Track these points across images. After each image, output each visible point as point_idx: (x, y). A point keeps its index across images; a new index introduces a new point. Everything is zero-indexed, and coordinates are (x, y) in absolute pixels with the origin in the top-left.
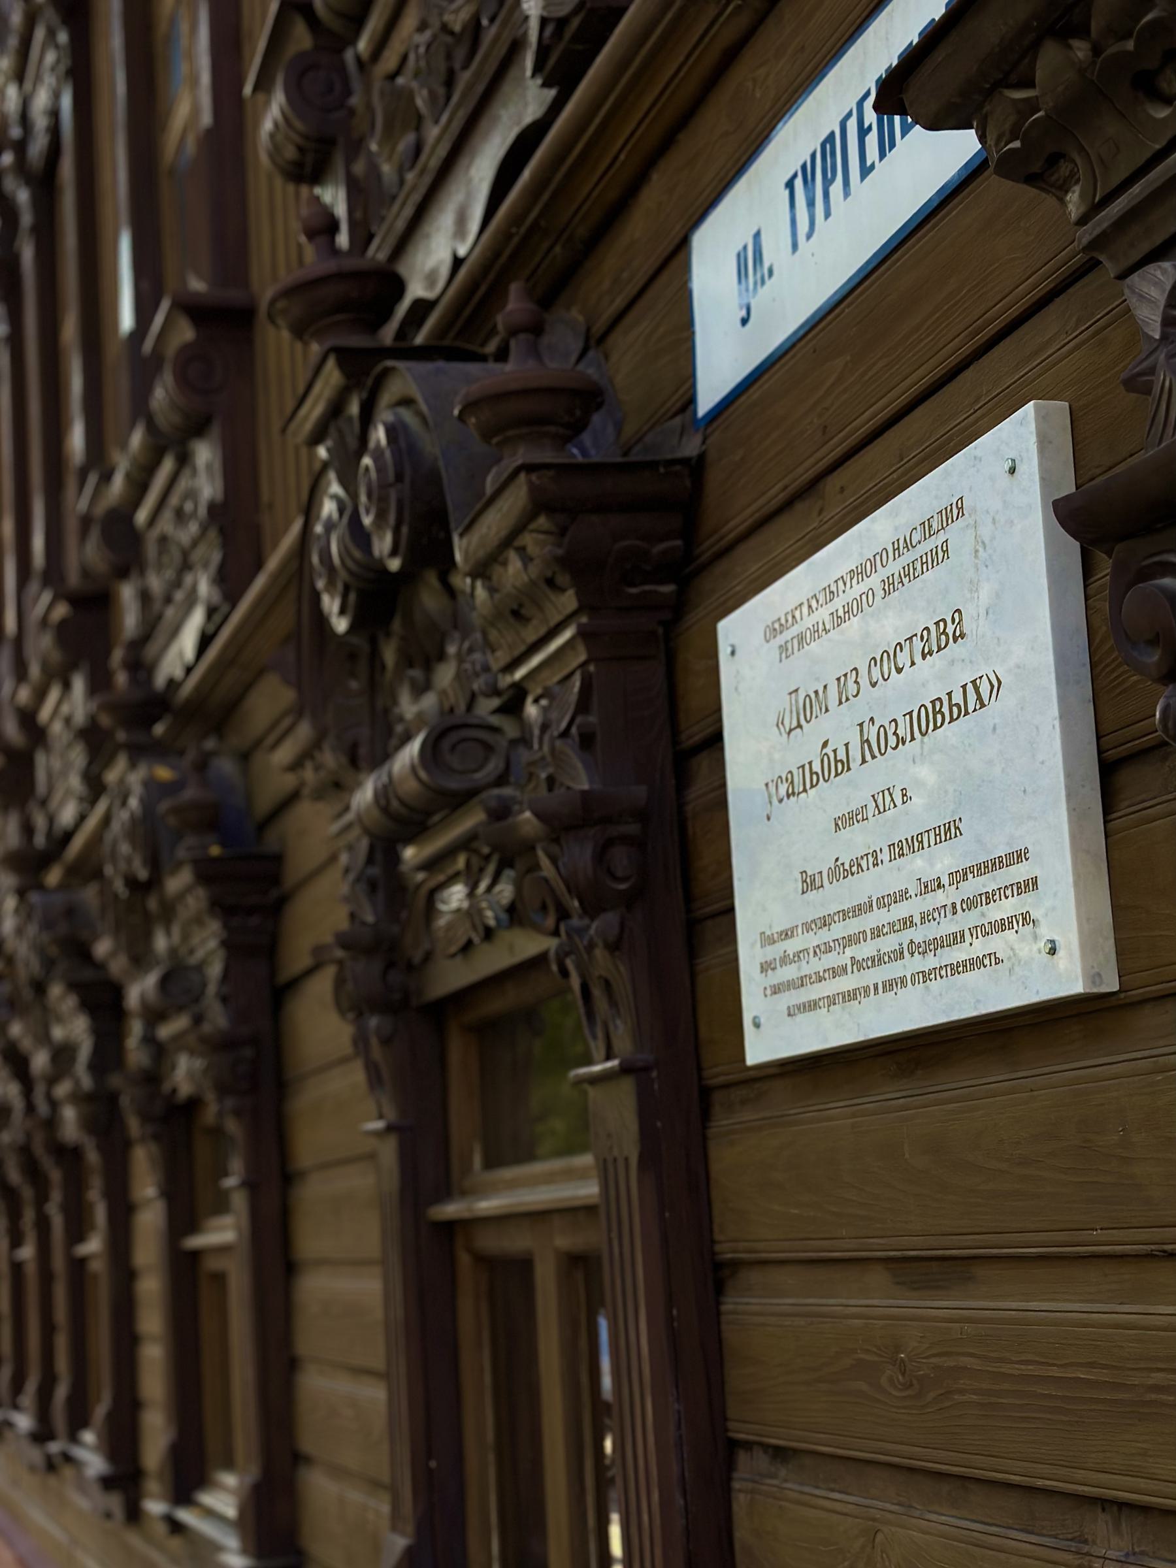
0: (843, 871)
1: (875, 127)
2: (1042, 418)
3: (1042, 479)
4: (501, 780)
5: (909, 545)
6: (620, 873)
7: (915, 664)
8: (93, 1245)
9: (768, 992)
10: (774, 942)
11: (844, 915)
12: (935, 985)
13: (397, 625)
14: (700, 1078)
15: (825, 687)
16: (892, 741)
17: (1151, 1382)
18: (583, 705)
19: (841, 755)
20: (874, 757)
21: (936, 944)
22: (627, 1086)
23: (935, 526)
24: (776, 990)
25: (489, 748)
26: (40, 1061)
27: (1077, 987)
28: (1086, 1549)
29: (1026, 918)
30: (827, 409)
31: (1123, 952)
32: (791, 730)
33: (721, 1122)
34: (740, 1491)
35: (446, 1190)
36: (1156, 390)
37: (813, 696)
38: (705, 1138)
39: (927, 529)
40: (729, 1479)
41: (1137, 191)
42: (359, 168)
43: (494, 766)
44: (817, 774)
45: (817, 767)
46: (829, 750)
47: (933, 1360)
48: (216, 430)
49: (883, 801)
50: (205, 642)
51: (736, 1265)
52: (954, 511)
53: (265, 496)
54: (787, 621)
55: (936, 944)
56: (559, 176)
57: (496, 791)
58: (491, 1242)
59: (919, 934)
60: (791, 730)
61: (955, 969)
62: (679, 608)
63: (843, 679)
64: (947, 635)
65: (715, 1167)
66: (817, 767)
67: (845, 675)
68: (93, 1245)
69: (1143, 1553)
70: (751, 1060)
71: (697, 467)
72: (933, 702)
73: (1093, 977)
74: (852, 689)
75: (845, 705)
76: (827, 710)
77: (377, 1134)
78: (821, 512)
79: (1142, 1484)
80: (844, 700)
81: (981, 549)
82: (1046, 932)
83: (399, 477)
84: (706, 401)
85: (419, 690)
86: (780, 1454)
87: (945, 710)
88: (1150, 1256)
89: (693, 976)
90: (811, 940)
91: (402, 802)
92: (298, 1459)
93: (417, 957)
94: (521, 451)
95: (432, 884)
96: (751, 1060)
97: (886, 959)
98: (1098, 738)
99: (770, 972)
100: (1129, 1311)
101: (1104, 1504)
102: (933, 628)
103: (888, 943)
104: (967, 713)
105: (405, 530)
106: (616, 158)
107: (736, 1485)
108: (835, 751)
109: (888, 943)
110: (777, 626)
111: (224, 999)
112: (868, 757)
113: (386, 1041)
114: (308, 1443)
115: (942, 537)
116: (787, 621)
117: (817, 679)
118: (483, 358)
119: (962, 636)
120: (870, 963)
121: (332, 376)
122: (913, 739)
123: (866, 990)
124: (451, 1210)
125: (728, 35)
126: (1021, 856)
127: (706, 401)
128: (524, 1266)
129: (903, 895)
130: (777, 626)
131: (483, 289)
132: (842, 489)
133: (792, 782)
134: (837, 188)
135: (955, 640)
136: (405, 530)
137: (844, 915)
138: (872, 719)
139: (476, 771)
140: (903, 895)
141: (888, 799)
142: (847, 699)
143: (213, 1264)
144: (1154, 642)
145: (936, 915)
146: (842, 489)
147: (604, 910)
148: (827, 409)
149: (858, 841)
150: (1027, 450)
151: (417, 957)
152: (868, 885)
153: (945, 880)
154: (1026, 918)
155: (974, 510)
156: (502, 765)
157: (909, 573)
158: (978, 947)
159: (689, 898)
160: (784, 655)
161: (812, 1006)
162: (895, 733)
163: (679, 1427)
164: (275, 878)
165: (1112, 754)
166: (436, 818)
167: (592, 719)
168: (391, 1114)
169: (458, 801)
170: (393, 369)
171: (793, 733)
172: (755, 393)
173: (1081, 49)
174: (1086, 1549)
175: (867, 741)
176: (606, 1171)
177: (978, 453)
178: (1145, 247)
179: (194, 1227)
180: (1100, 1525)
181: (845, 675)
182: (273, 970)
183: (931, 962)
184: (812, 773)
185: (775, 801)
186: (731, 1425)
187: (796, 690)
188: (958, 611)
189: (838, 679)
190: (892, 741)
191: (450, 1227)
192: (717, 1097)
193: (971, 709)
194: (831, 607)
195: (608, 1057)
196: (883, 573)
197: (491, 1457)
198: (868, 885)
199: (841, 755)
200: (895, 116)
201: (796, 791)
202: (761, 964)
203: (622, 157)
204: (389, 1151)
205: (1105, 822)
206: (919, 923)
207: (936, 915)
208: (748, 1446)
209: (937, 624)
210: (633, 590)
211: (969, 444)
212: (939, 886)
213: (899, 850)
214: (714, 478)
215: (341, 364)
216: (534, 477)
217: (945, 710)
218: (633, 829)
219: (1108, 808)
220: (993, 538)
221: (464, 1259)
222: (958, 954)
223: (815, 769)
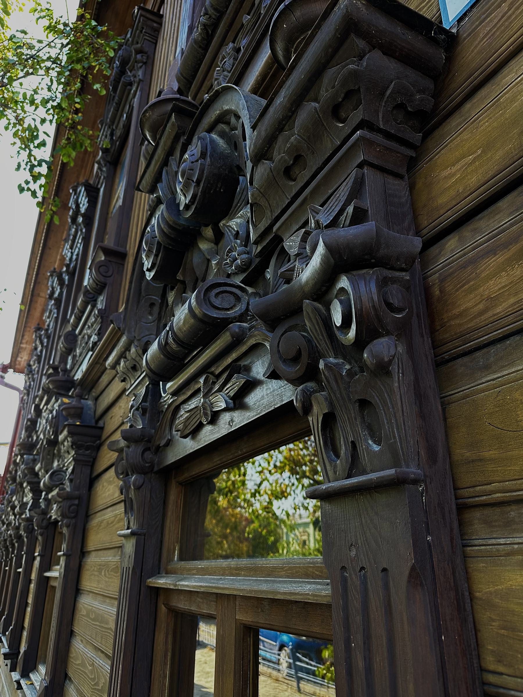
7: (150, 442)
8: (55, 573)
25: (238, 299)
26: (45, 479)
35: (157, 571)
58: (183, 605)
68: (55, 573)
77: (125, 536)
111: (71, 481)
113: (138, 488)
124: (162, 582)
143: (53, 583)
166: (54, 488)
167: (148, 404)
168: (134, 526)
179: (49, 569)
191: (157, 591)
195: (128, 529)
204: (130, 547)
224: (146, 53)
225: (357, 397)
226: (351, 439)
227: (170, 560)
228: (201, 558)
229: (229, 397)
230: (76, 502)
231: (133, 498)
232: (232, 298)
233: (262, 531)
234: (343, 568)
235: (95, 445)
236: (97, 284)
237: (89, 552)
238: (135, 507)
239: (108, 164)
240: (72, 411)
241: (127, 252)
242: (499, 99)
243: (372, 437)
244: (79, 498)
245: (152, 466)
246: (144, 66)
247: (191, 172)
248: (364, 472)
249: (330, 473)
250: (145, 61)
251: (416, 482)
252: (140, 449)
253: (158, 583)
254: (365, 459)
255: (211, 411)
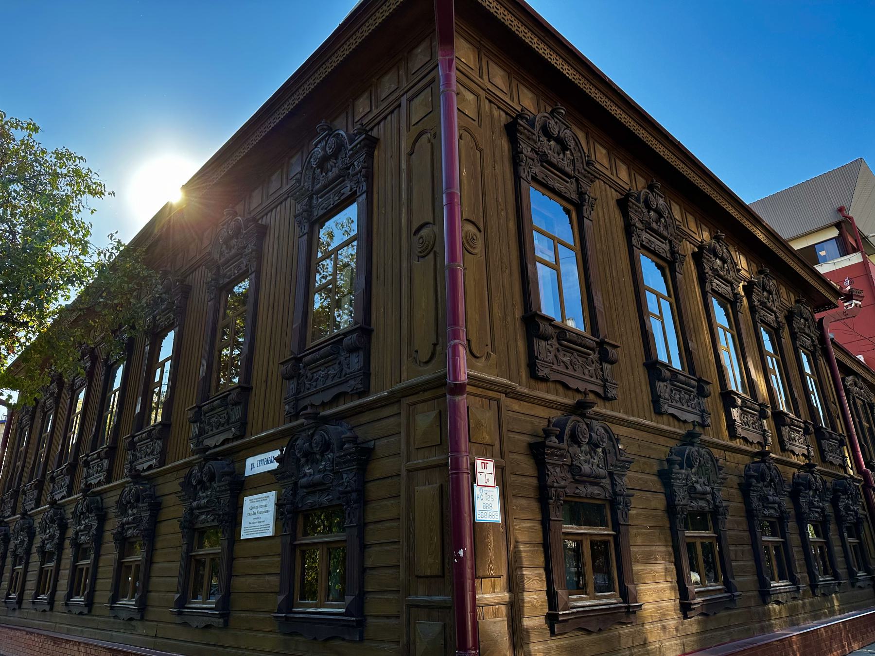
22: (227, 541)
49: (258, 518)
51: (235, 558)
52: (268, 497)
71: (244, 481)
84: (245, 475)
127: (245, 475)
128: (83, 569)
149: (256, 521)
152: (256, 524)
170: (290, 356)
176: (222, 549)
191: (192, 556)
198: (256, 524)
200: (248, 472)
211: (644, 347)
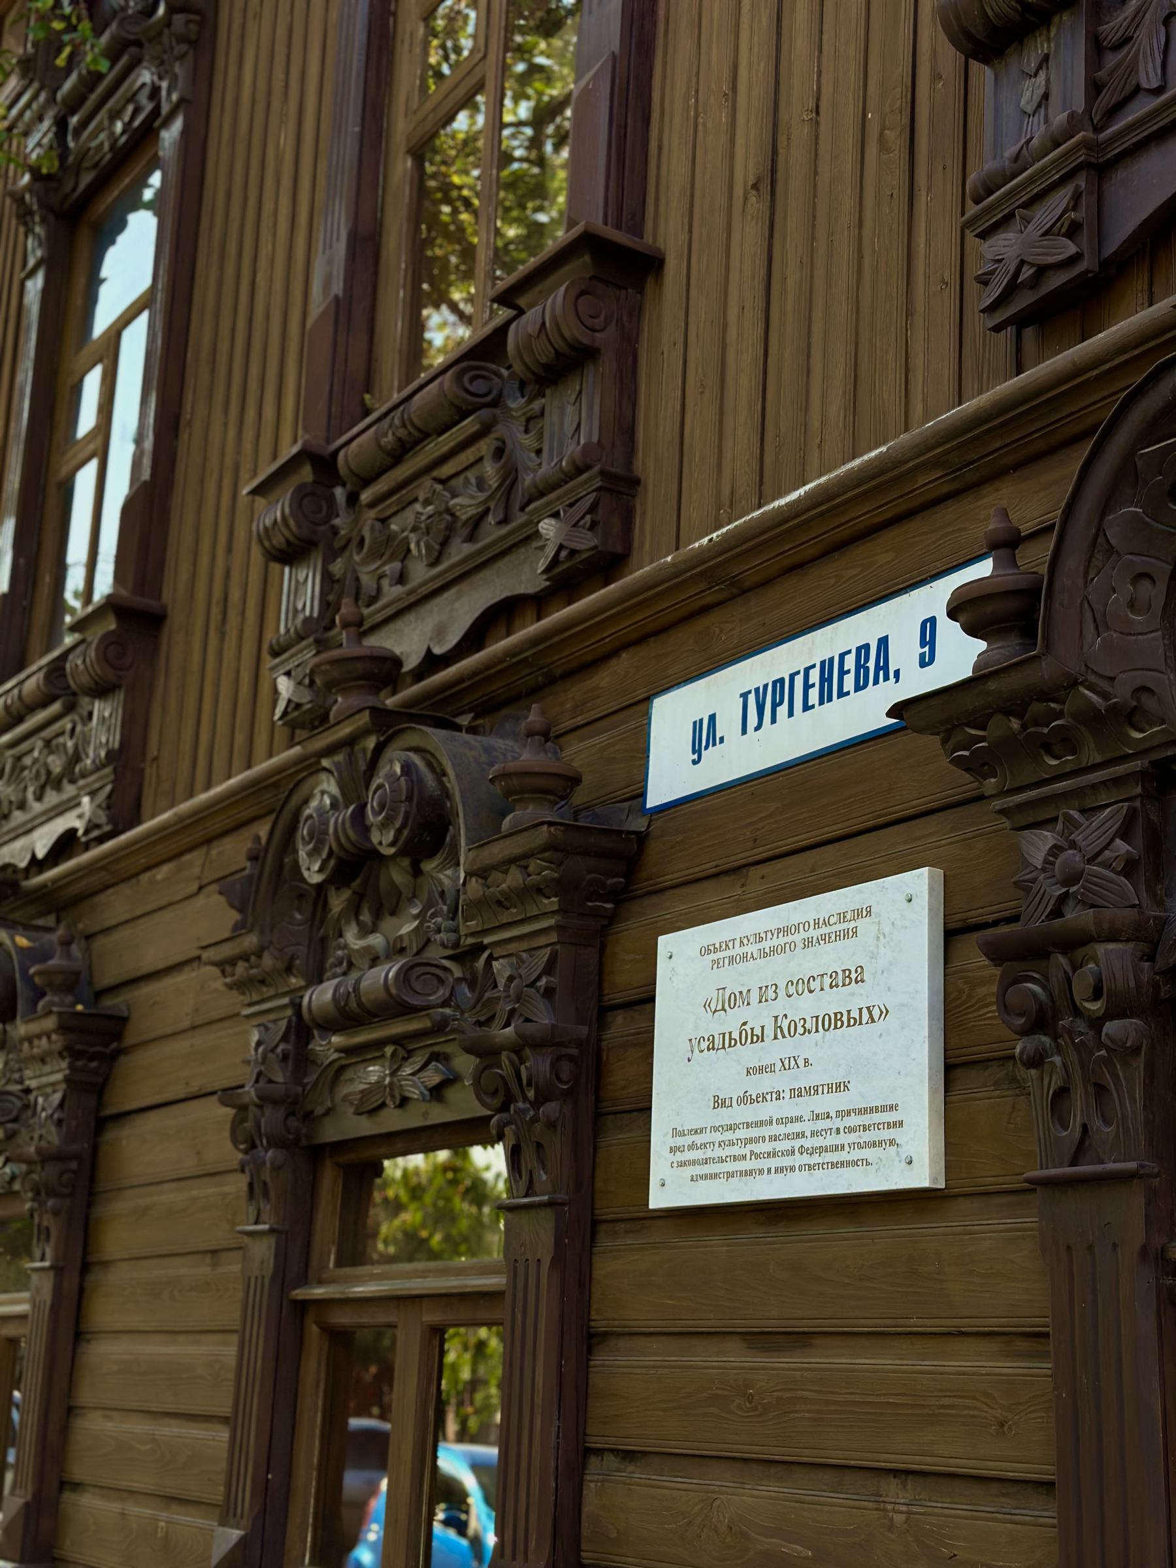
0: (746, 1099)
1: (817, 685)
2: (931, 877)
3: (929, 909)
4: (445, 1004)
5: (826, 923)
6: (564, 1077)
9: (675, 1165)
10: (684, 1135)
11: (748, 1125)
12: (817, 1173)
13: (356, 884)
14: (593, 1214)
15: (749, 991)
16: (800, 1030)
17: (941, 1403)
18: (548, 970)
19: (758, 1031)
20: (784, 1037)
21: (822, 1150)
22: (271, 1241)
23: (848, 917)
24: (682, 1164)
25: (441, 981)
27: (926, 1184)
28: (881, 1499)
29: (892, 1142)
30: (758, 829)
31: (949, 1168)
32: (715, 1011)
33: (604, 1243)
34: (591, 1481)
35: (304, 1280)
36: (1033, 892)
37: (738, 994)
38: (591, 1254)
39: (842, 917)
40: (583, 1474)
41: (1033, 793)
42: (337, 567)
43: (442, 993)
44: (735, 1040)
45: (736, 1035)
46: (747, 1027)
47: (775, 1394)
48: (120, 696)
50: (66, 844)
51: (605, 1336)
53: (152, 751)
54: (721, 947)
55: (822, 1150)
56: (556, 639)
57: (441, 1010)
58: (342, 1318)
59: (808, 1143)
60: (715, 1011)
61: (834, 1165)
62: (613, 919)
63: (764, 989)
64: (851, 979)
65: (597, 1274)
66: (736, 1035)
67: (767, 987)
69: (921, 1500)
70: (653, 1205)
71: (642, 838)
72: (836, 1014)
73: (934, 1180)
74: (771, 995)
75: (764, 1004)
76: (748, 1004)
78: (743, 885)
79: (929, 1459)
80: (763, 1000)
81: (882, 937)
82: (905, 1152)
83: (409, 798)
85: (365, 931)
86: (629, 1456)
87: (845, 1019)
88: (949, 1334)
89: (595, 1149)
90: (718, 1137)
91: (360, 1004)
92: (66, 1485)
93: (319, 1111)
94: (531, 807)
95: (344, 1062)
96: (653, 1205)
97: (780, 1154)
98: (945, 1050)
99: (678, 1153)
100: (927, 1364)
101: (895, 1472)
102: (840, 973)
103: (785, 1145)
104: (861, 1023)
105: (406, 832)
106: (603, 639)
107: (588, 1478)
108: (752, 1029)
109: (785, 1145)
110: (712, 948)
112: (779, 1036)
114: (78, 1471)
115: (853, 924)
116: (721, 947)
117: (743, 985)
118: (458, 728)
119: (862, 981)
120: (766, 1156)
121: (364, 718)
122: (817, 1031)
123: (761, 1172)
124: (299, 1294)
125: (709, 599)
126: (892, 1108)
129: (799, 1119)
130: (712, 948)
131: (465, 685)
132: (763, 877)
133: (713, 1042)
134: (783, 710)
135: (857, 982)
136: (406, 832)
137: (748, 1125)
138: (785, 1016)
139: (430, 995)
140: (799, 1119)
141: (793, 1062)
142: (766, 1001)
144: (1021, 1015)
145: (823, 1133)
146: (763, 877)
147: (550, 1100)
148: (758, 829)
149: (766, 1083)
150: (921, 892)
151: (319, 1111)
153: (833, 1114)
154: (892, 1142)
155: (878, 915)
156: (448, 994)
157: (824, 938)
158: (856, 1154)
159: (598, 1100)
160: (715, 966)
161: (715, 1176)
162: (803, 1026)
163: (558, 1438)
164: (118, 1036)
165: (952, 1061)
169: (407, 1010)
171: (717, 1013)
172: (698, 805)
173: (1015, 724)
174: (881, 1499)
175: (780, 1027)
177: (885, 885)
178: (1031, 820)
180: (891, 1486)
181: (767, 987)
182: (100, 1104)
183: (816, 1159)
184: (730, 1039)
185: (696, 1050)
186: (588, 1439)
187: (724, 988)
188: (861, 967)
189: (761, 988)
190: (800, 1030)
192: (603, 1228)
193: (864, 1021)
194: (760, 946)
196: (803, 935)
197: (315, 1474)
199: (758, 1031)
201: (716, 1047)
202: (671, 1147)
203: (607, 640)
205: (945, 1096)
206: (809, 1136)
207: (823, 1133)
208: (600, 1452)
209: (844, 971)
210: (590, 904)
212: (828, 1117)
213: (797, 1093)
214: (654, 848)
215: (371, 713)
216: (552, 829)
217: (845, 1019)
218: (574, 1052)
219: (946, 1091)
220: (891, 933)
221: (313, 1330)
222: (843, 1156)
223: (733, 1036)
224: (198, 12)
225: (535, 1140)
226: (529, 1168)
227: (324, 1266)
228: (363, 1264)
229: (425, 1087)
230: (73, 1165)
231: (268, 1180)
232: (435, 982)
233: (431, 1235)
234: (516, 1260)
235: (108, 1051)
236: (96, 683)
237: (106, 1264)
238: (272, 1194)
239: (51, 218)
240: (59, 979)
241: (165, 608)
242: (656, 922)
243: (543, 1169)
244: (77, 1157)
245: (297, 1141)
246: (191, 53)
247: (392, 813)
248: (535, 1195)
249: (515, 1191)
250: (193, 37)
251: (563, 1204)
252: (280, 1113)
253: (314, 1294)
254: (537, 1186)
255: (401, 1095)
